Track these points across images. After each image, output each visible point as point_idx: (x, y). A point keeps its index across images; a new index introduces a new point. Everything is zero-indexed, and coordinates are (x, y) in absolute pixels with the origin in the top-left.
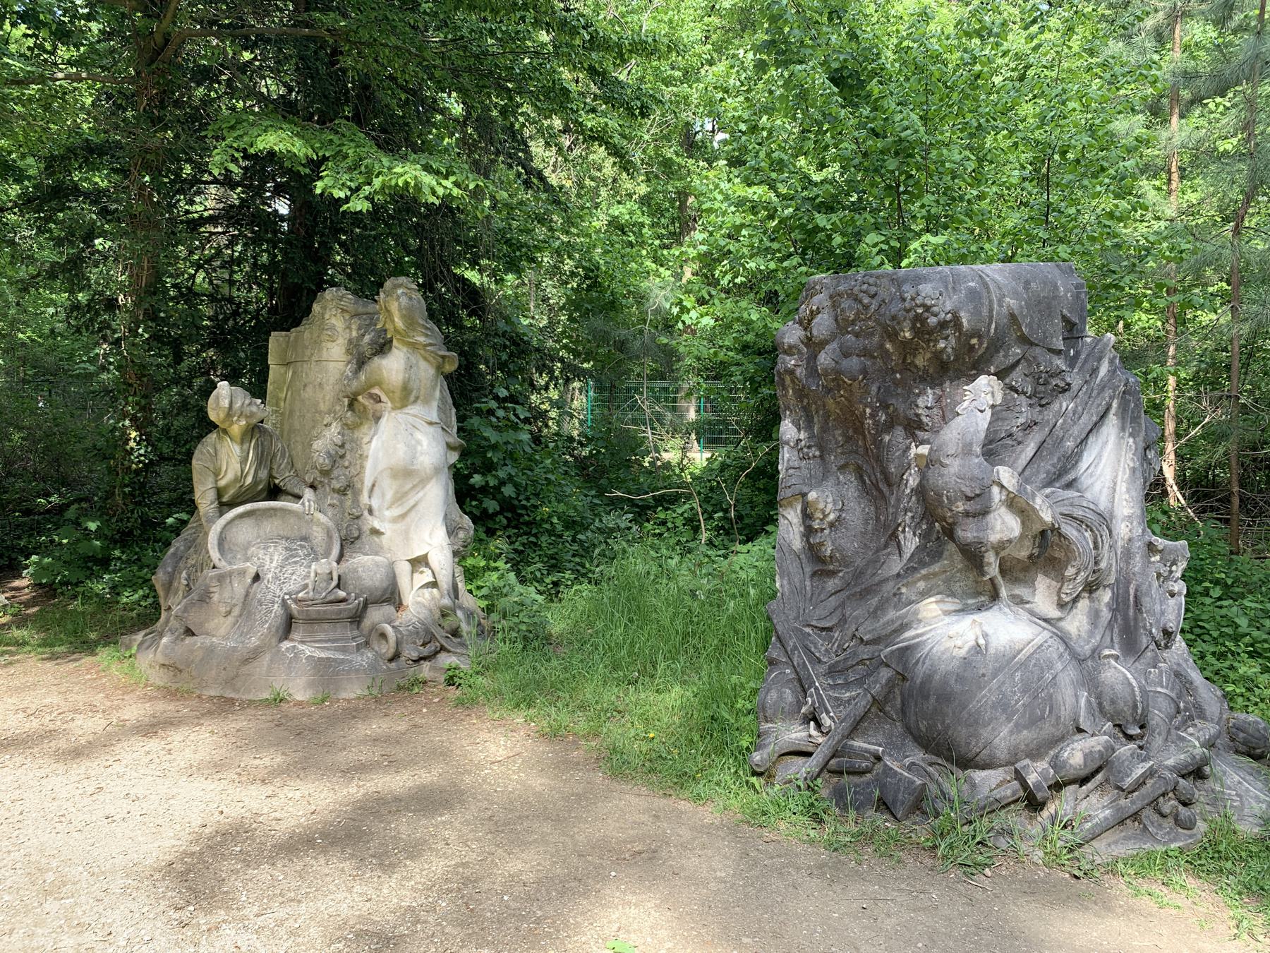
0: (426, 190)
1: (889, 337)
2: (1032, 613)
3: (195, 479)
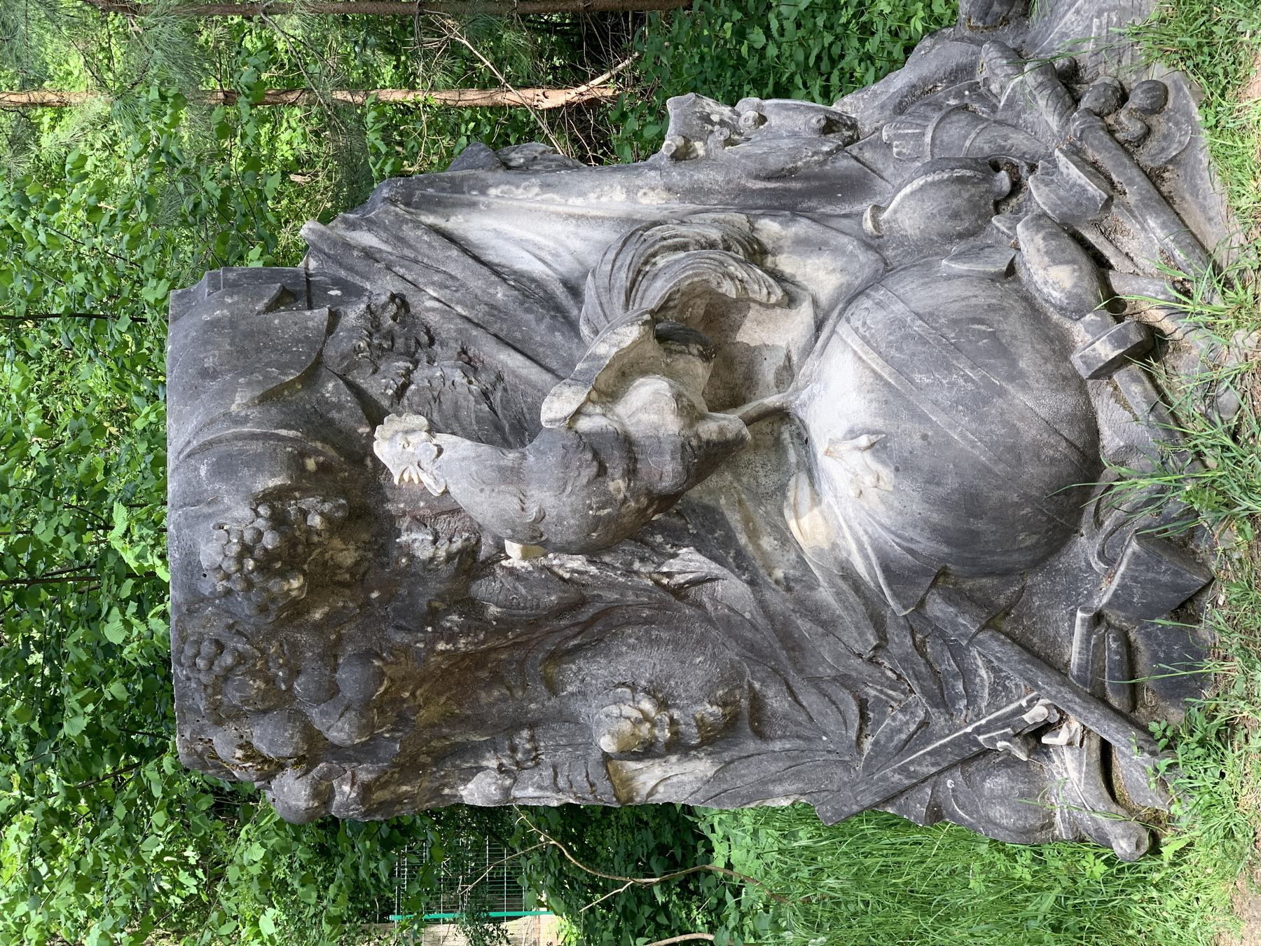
1: (300, 614)
2: (807, 351)
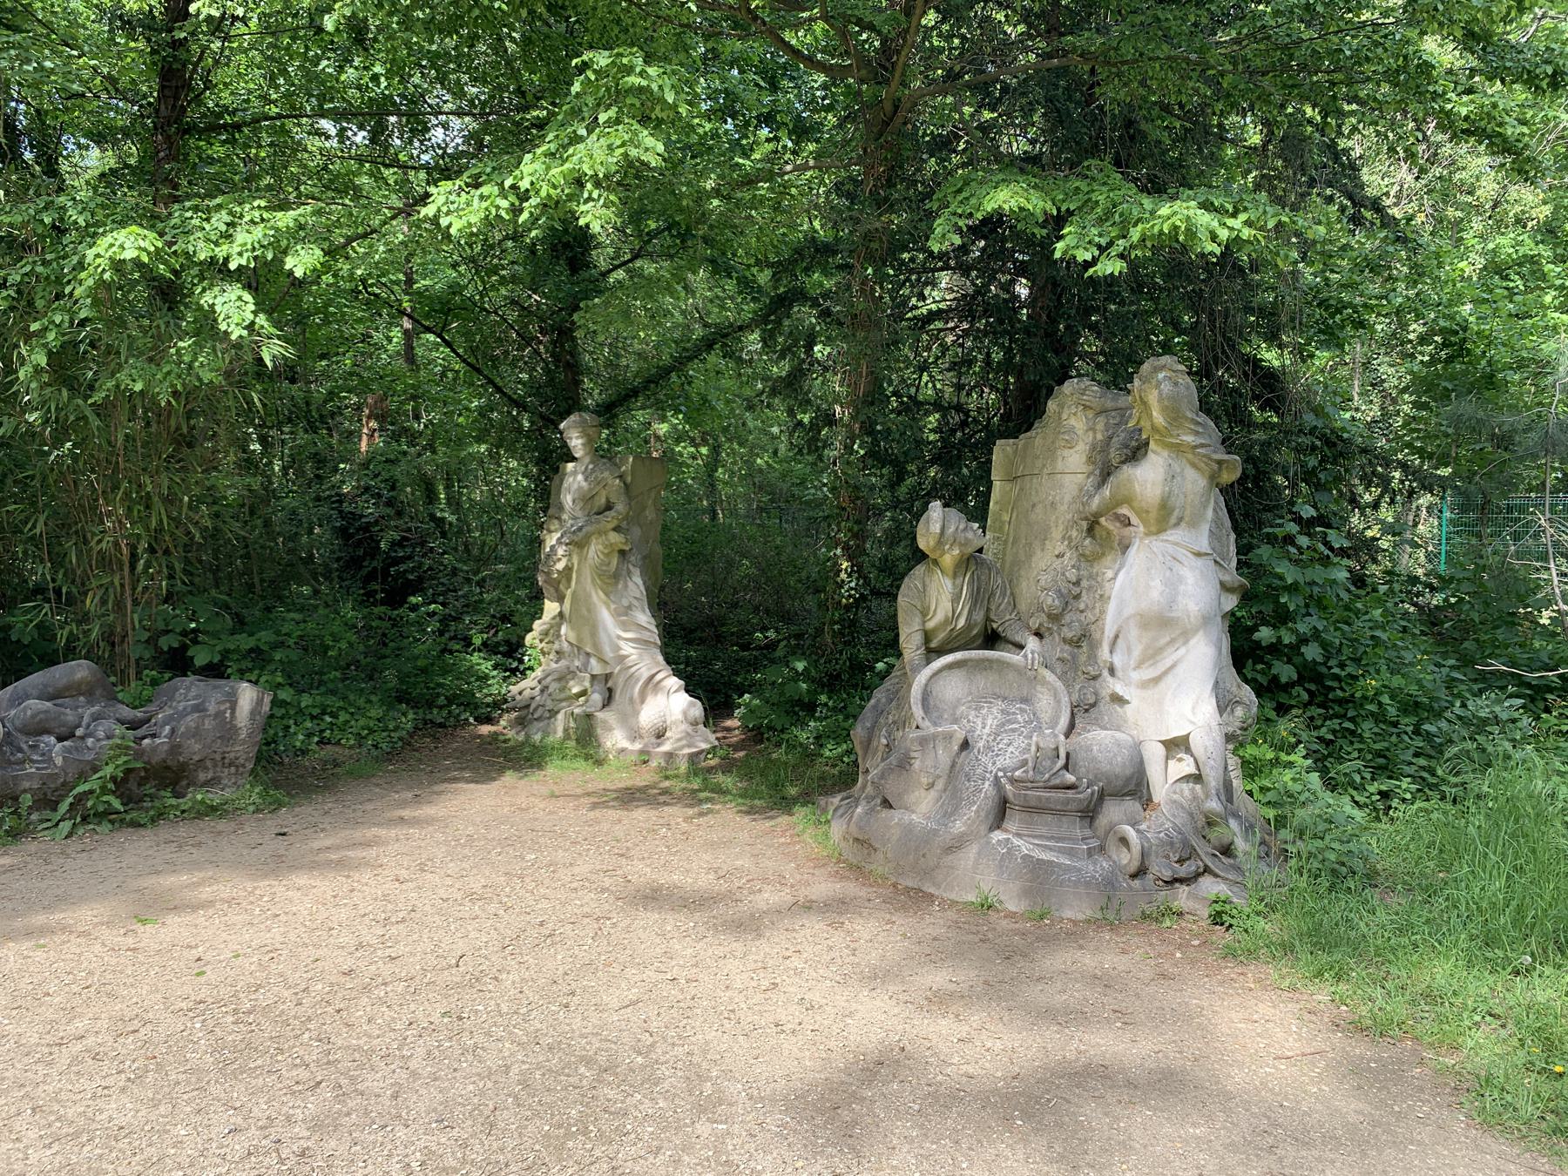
0: (1203, 235)
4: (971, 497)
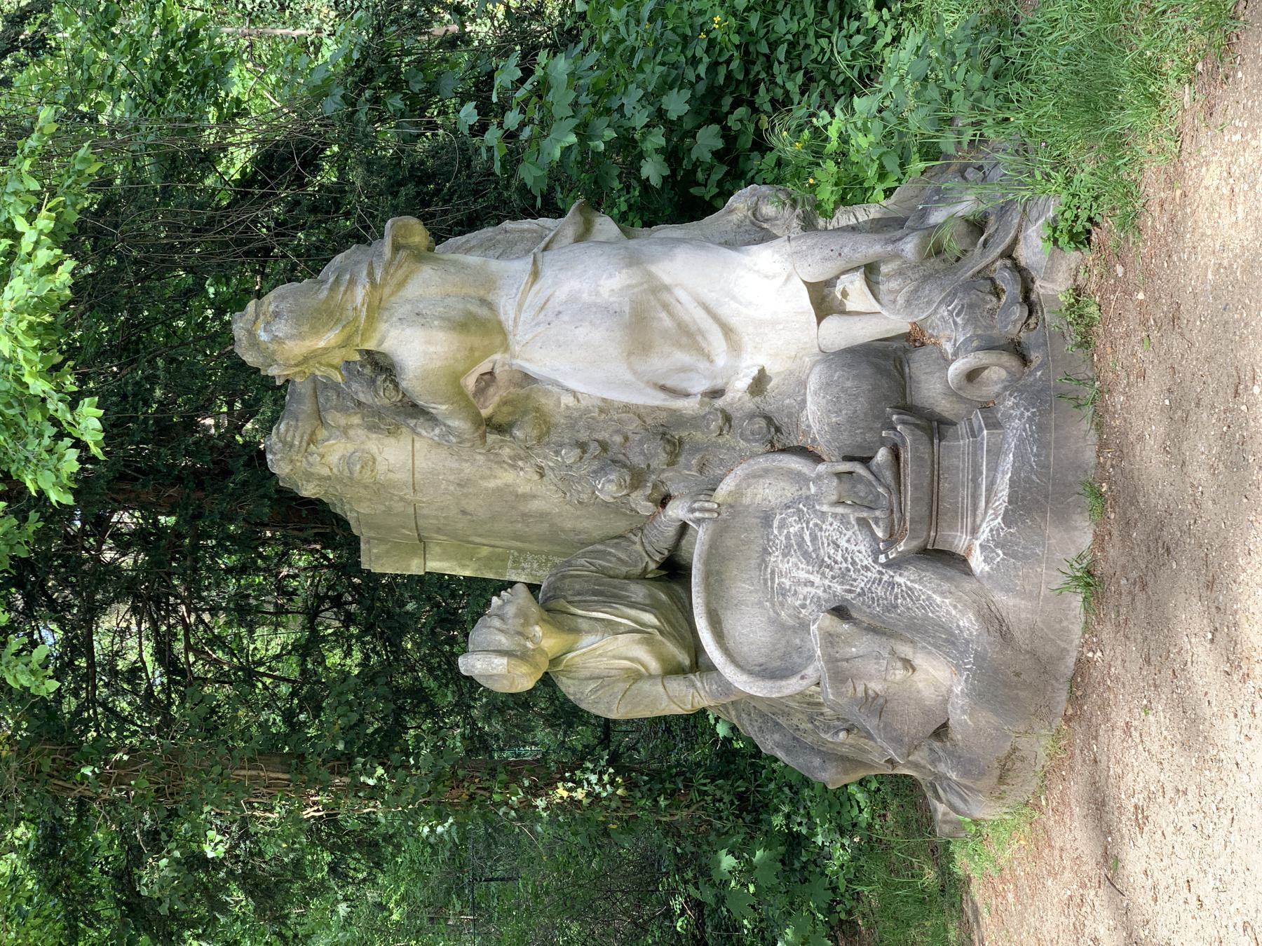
0: (42, 287)
3: (648, 714)
4: (456, 606)
